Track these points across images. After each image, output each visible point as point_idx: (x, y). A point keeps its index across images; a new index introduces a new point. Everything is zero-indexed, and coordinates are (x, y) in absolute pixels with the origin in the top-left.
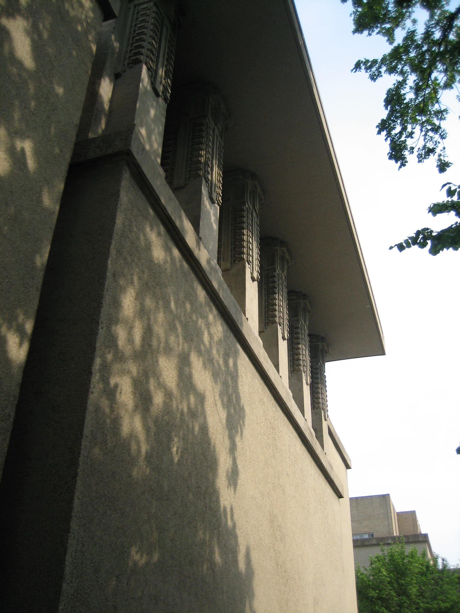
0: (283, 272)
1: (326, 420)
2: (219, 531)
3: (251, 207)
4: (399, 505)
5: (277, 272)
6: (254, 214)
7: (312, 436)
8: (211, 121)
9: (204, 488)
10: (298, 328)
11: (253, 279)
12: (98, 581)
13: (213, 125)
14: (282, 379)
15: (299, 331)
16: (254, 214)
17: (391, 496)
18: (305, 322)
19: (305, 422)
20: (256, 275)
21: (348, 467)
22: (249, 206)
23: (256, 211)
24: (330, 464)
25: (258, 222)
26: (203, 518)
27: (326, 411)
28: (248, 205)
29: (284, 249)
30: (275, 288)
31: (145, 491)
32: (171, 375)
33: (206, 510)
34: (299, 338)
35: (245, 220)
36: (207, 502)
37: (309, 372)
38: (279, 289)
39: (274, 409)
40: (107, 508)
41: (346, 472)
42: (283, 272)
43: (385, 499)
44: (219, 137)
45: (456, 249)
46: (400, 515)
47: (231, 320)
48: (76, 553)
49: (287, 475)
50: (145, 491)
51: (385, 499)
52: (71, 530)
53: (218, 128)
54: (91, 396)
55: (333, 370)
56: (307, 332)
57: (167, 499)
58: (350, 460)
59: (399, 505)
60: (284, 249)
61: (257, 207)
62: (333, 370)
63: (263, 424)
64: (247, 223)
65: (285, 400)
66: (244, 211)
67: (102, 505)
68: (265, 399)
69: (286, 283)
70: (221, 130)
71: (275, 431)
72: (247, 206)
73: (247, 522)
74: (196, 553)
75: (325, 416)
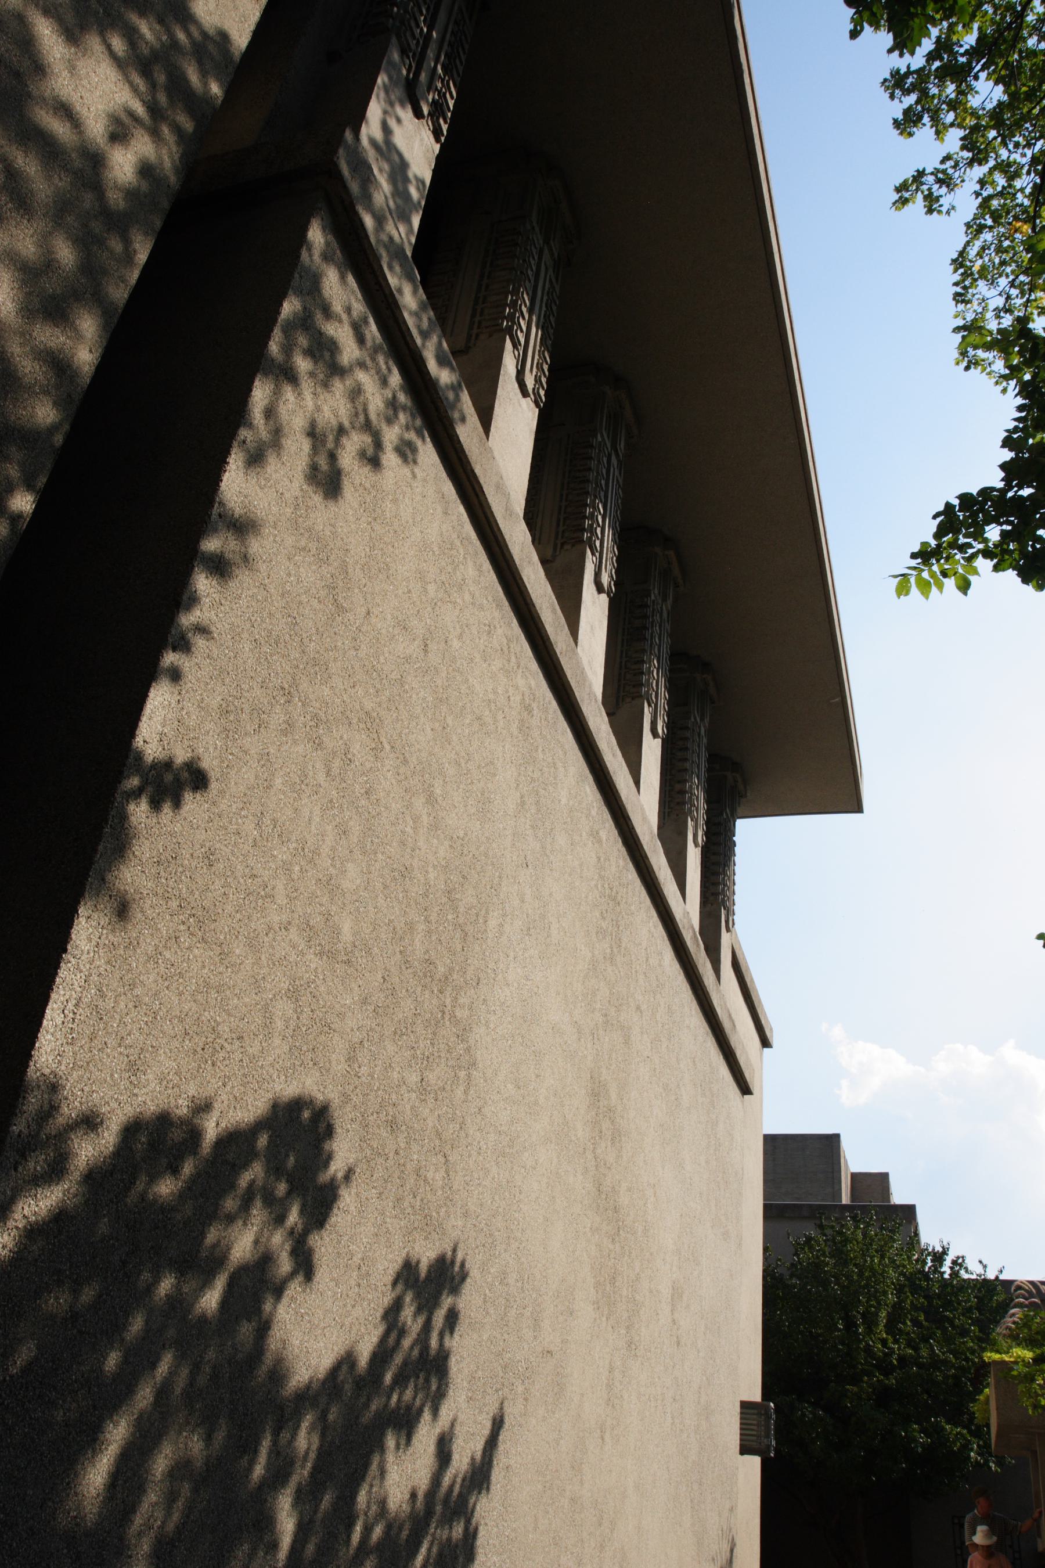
0: (664, 600)
1: (728, 930)
2: (469, 1076)
3: (609, 445)
4: (856, 1159)
5: (653, 597)
6: (614, 461)
7: (698, 945)
8: (537, 229)
9: (441, 969)
10: (687, 728)
11: (600, 588)
12: (136, 1095)
13: (541, 242)
14: (645, 804)
15: (687, 765)
16: (614, 461)
17: (842, 1138)
18: (702, 720)
19: (688, 910)
20: (605, 579)
21: (765, 1043)
22: (603, 439)
23: (617, 455)
24: (730, 1015)
25: (621, 481)
26: (434, 1034)
27: (730, 912)
28: (602, 437)
29: (671, 553)
30: (646, 628)
31: (289, 923)
32: (387, 693)
33: (443, 1018)
34: (687, 749)
35: (593, 464)
36: (448, 1001)
37: (701, 822)
38: (652, 643)
39: (621, 863)
40: (182, 928)
41: (761, 1054)
42: (664, 600)
43: (830, 1144)
44: (550, 272)
45: (1040, 588)
46: (857, 1178)
47: (542, 638)
48: (76, 1005)
49: (638, 1008)
50: (289, 923)
51: (830, 1144)
52: (69, 947)
53: (550, 249)
54: (403, 1313)
55: (754, 836)
56: (705, 740)
57: (348, 962)
58: (771, 1029)
59: (856, 1159)
60: (671, 553)
61: (622, 446)
62: (754, 836)
63: (594, 882)
64: (598, 473)
65: (645, 847)
66: (592, 446)
67: (168, 917)
68: (603, 835)
69: (668, 627)
70: (556, 255)
71: (618, 909)
72: (599, 439)
73: (538, 1076)
74: (408, 1107)
75: (727, 922)
